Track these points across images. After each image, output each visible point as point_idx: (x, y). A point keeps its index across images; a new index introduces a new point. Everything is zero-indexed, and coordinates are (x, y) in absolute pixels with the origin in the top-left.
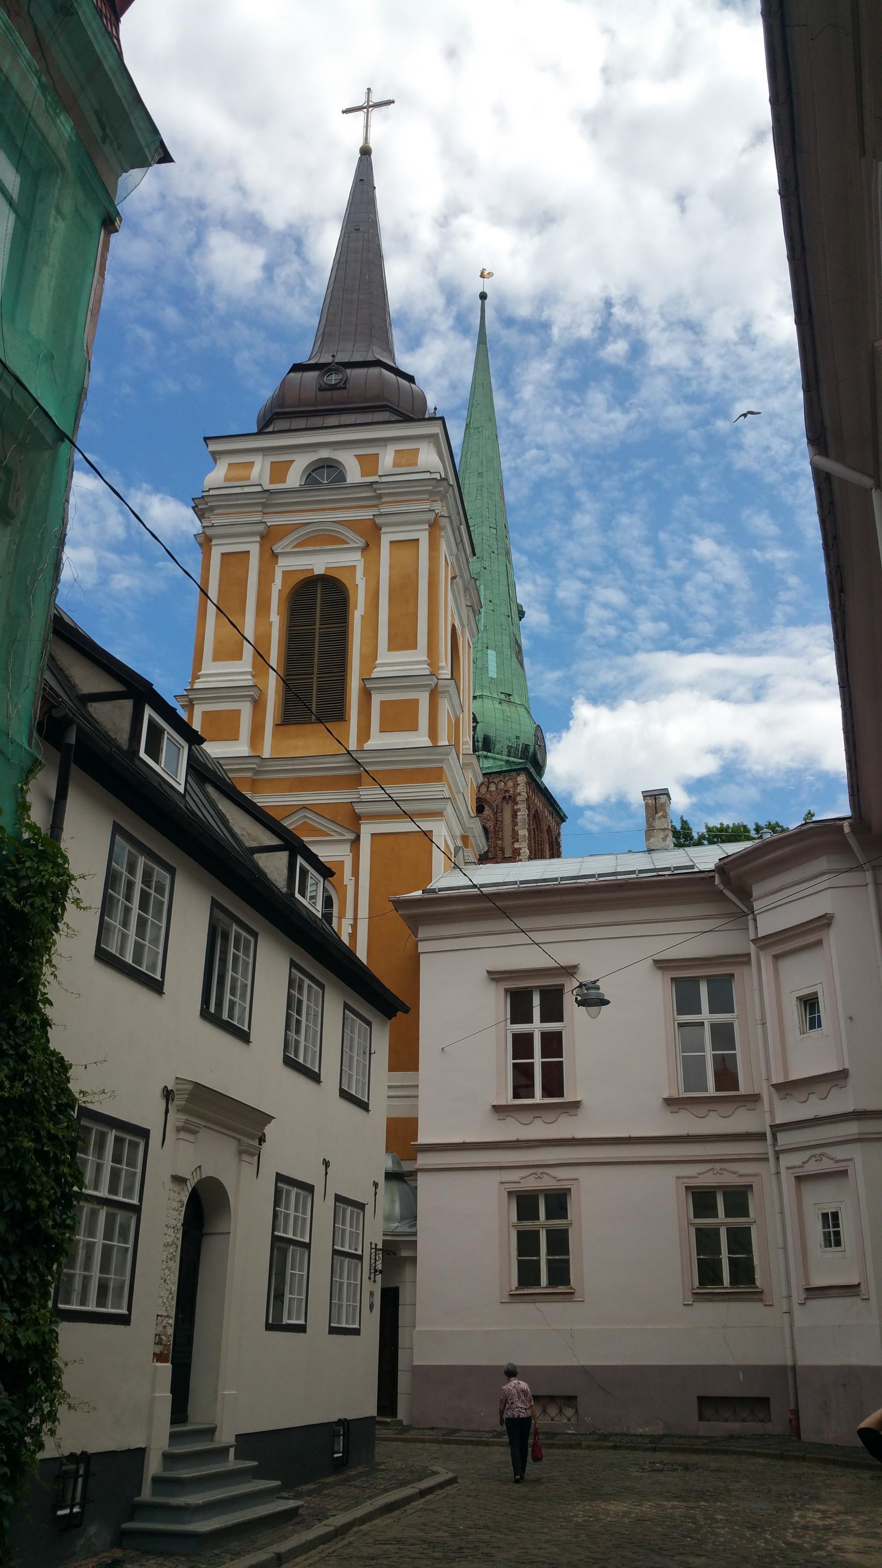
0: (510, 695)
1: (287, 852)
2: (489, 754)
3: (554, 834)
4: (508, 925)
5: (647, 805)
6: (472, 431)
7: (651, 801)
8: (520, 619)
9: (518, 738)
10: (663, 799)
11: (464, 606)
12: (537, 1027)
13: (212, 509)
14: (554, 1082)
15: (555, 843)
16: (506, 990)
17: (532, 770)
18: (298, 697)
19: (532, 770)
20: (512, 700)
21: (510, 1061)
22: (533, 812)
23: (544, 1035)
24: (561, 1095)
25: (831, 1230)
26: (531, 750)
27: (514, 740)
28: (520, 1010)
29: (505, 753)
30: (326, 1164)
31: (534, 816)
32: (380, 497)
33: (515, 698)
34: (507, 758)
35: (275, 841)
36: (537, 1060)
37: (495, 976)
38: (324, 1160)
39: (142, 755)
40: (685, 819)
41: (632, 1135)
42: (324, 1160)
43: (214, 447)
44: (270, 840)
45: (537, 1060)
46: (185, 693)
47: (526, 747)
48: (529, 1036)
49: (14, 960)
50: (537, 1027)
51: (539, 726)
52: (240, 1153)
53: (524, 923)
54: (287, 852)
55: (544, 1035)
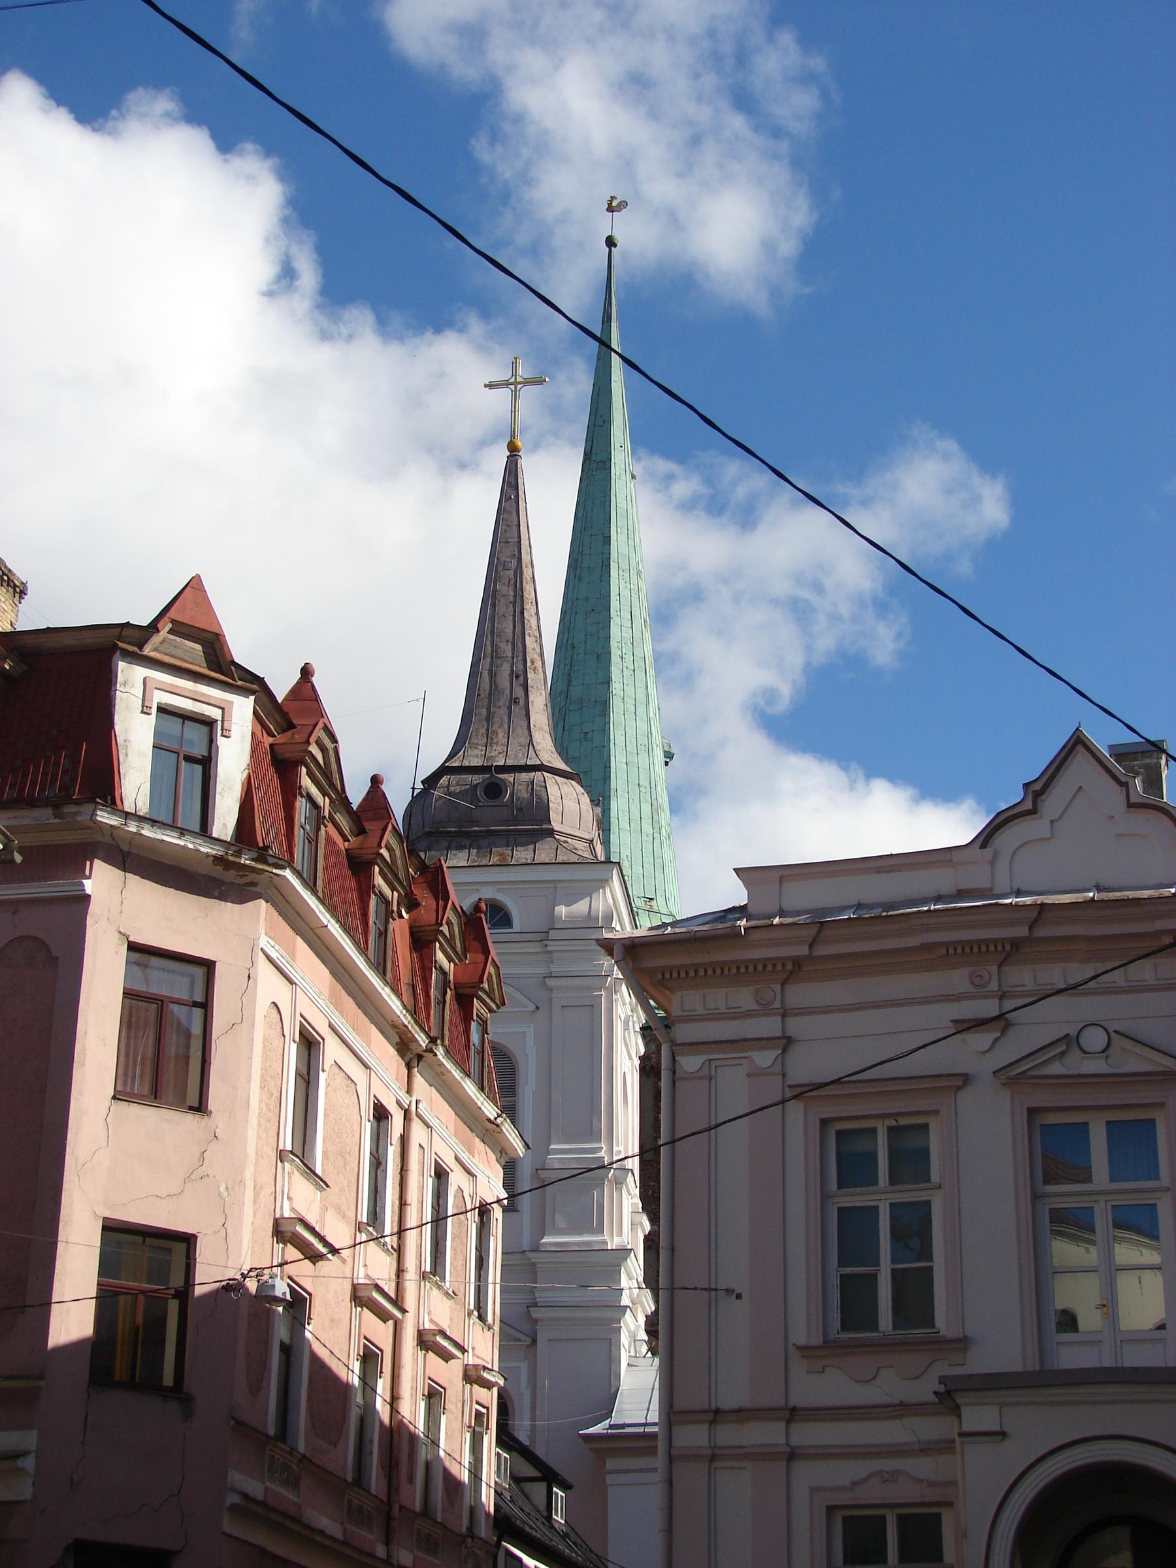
0: (651, 899)
25: (881, 1198)
50: (881, 1198)
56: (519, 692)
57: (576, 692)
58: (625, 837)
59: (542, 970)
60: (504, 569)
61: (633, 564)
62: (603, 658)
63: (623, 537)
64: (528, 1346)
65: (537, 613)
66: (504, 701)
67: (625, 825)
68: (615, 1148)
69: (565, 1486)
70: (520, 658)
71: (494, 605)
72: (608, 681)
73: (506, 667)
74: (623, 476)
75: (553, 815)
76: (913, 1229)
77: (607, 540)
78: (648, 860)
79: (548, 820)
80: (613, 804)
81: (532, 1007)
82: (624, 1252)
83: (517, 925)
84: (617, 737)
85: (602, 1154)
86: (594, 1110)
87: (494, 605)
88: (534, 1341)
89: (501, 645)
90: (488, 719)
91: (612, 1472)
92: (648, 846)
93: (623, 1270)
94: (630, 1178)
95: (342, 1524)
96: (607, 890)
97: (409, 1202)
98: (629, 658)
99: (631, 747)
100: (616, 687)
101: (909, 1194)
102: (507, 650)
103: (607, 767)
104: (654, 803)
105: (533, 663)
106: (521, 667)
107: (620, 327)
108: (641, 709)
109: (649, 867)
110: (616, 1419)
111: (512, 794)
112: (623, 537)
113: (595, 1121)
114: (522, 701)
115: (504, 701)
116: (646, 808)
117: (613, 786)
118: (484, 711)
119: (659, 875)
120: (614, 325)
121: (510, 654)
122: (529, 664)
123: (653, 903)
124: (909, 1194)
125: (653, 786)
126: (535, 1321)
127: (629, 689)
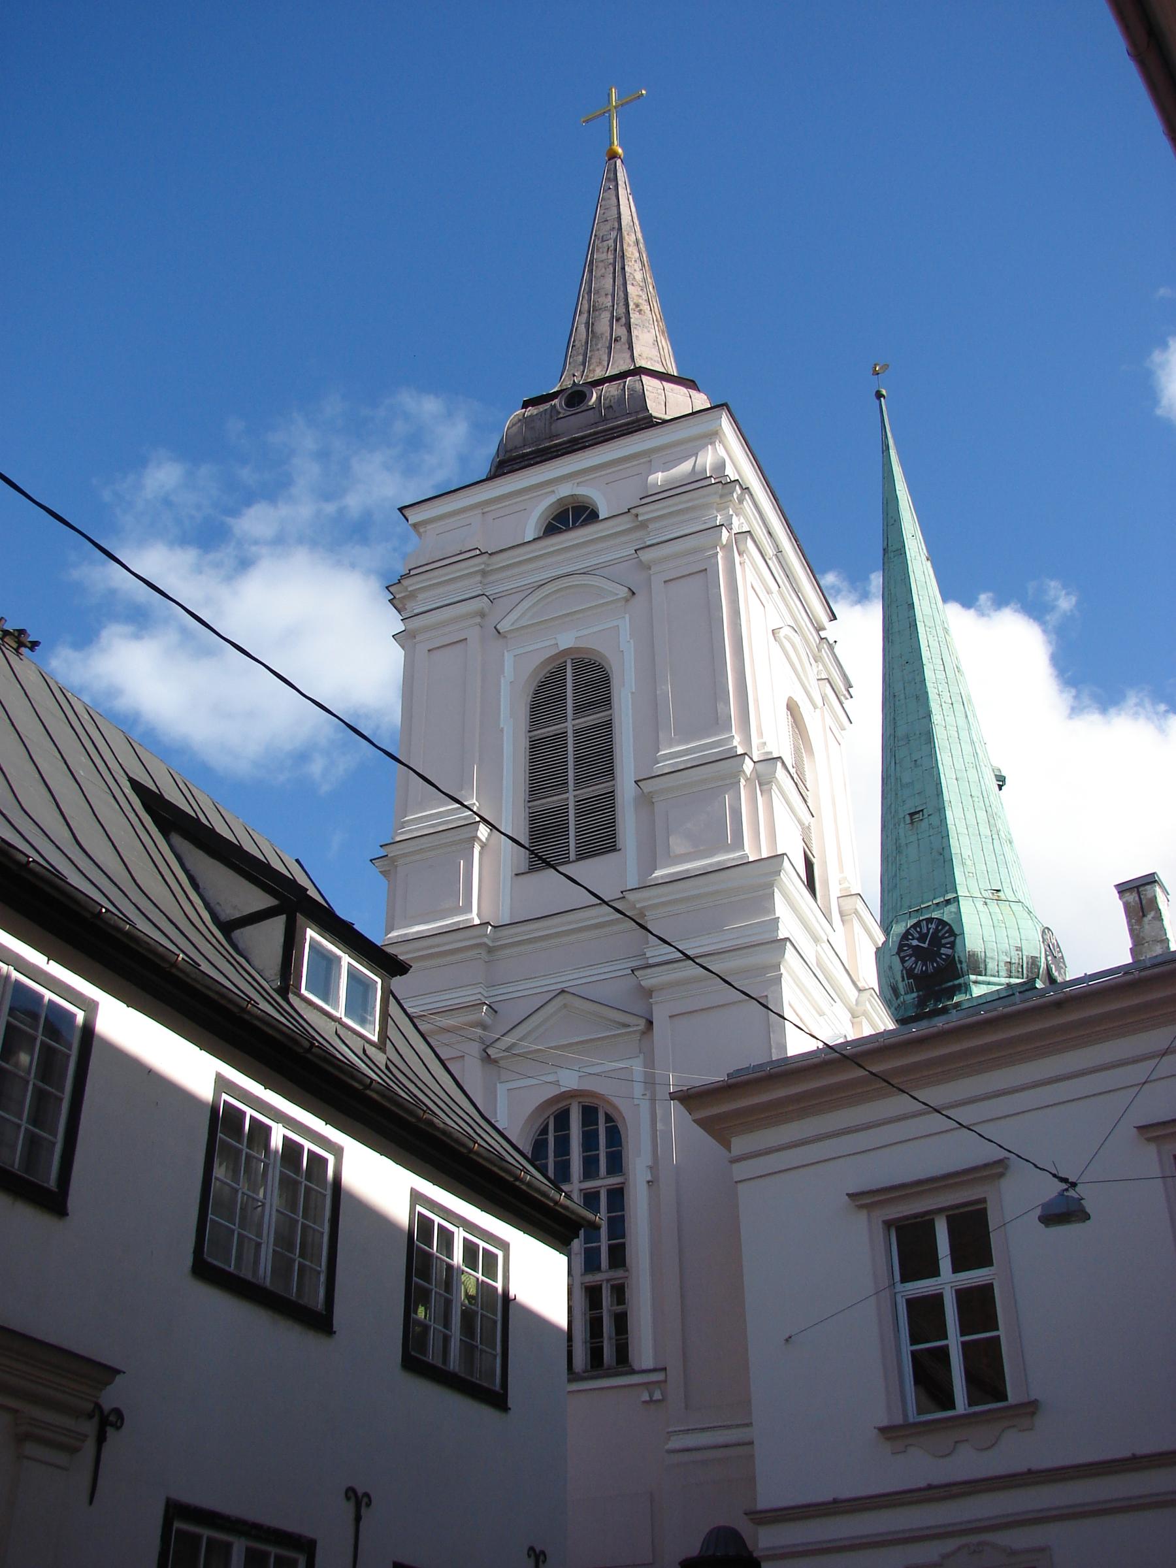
0: (998, 891)
2: (980, 978)
4: (899, 1104)
5: (1127, 907)
6: (892, 555)
7: (1132, 897)
8: (1000, 787)
9: (1019, 949)
10: (1148, 891)
11: (814, 682)
12: (947, 1281)
13: (412, 595)
14: (987, 1379)
16: (888, 1224)
20: (1003, 897)
23: (933, 1271)
26: (1043, 965)
27: (1014, 953)
28: (915, 1256)
29: (1003, 973)
30: (358, 1500)
32: (643, 525)
33: (1007, 893)
34: (1007, 980)
36: (954, 1341)
37: (864, 1200)
38: (532, 1549)
39: (379, 981)
42: (532, 1549)
43: (415, 516)
45: (954, 1341)
46: (382, 852)
47: (1034, 961)
48: (938, 1299)
50: (947, 1281)
52: (21, 1438)
53: (935, 1095)
55: (965, 1297)
56: (620, 331)
57: (901, 732)
58: (964, 840)
60: (603, 241)
61: (938, 622)
62: (922, 697)
63: (925, 603)
64: (643, 1033)
66: (603, 344)
67: (962, 829)
70: (622, 304)
71: (591, 271)
72: (928, 715)
73: (605, 317)
76: (978, 1307)
77: (911, 606)
78: (991, 859)
80: (949, 813)
81: (623, 592)
84: (944, 759)
86: (718, 692)
87: (591, 271)
88: (650, 1023)
90: (584, 364)
92: (988, 846)
93: (778, 896)
94: (780, 772)
98: (946, 695)
99: (959, 765)
100: (936, 718)
101: (974, 1277)
103: (939, 784)
104: (989, 809)
106: (622, 310)
107: (899, 453)
108: (964, 735)
109: (992, 865)
112: (925, 603)
113: (720, 706)
114: (624, 339)
115: (603, 344)
116: (982, 815)
117: (946, 797)
118: (580, 358)
119: (1003, 870)
120: (893, 453)
122: (632, 306)
124: (974, 1277)
126: (648, 993)
127: (950, 719)
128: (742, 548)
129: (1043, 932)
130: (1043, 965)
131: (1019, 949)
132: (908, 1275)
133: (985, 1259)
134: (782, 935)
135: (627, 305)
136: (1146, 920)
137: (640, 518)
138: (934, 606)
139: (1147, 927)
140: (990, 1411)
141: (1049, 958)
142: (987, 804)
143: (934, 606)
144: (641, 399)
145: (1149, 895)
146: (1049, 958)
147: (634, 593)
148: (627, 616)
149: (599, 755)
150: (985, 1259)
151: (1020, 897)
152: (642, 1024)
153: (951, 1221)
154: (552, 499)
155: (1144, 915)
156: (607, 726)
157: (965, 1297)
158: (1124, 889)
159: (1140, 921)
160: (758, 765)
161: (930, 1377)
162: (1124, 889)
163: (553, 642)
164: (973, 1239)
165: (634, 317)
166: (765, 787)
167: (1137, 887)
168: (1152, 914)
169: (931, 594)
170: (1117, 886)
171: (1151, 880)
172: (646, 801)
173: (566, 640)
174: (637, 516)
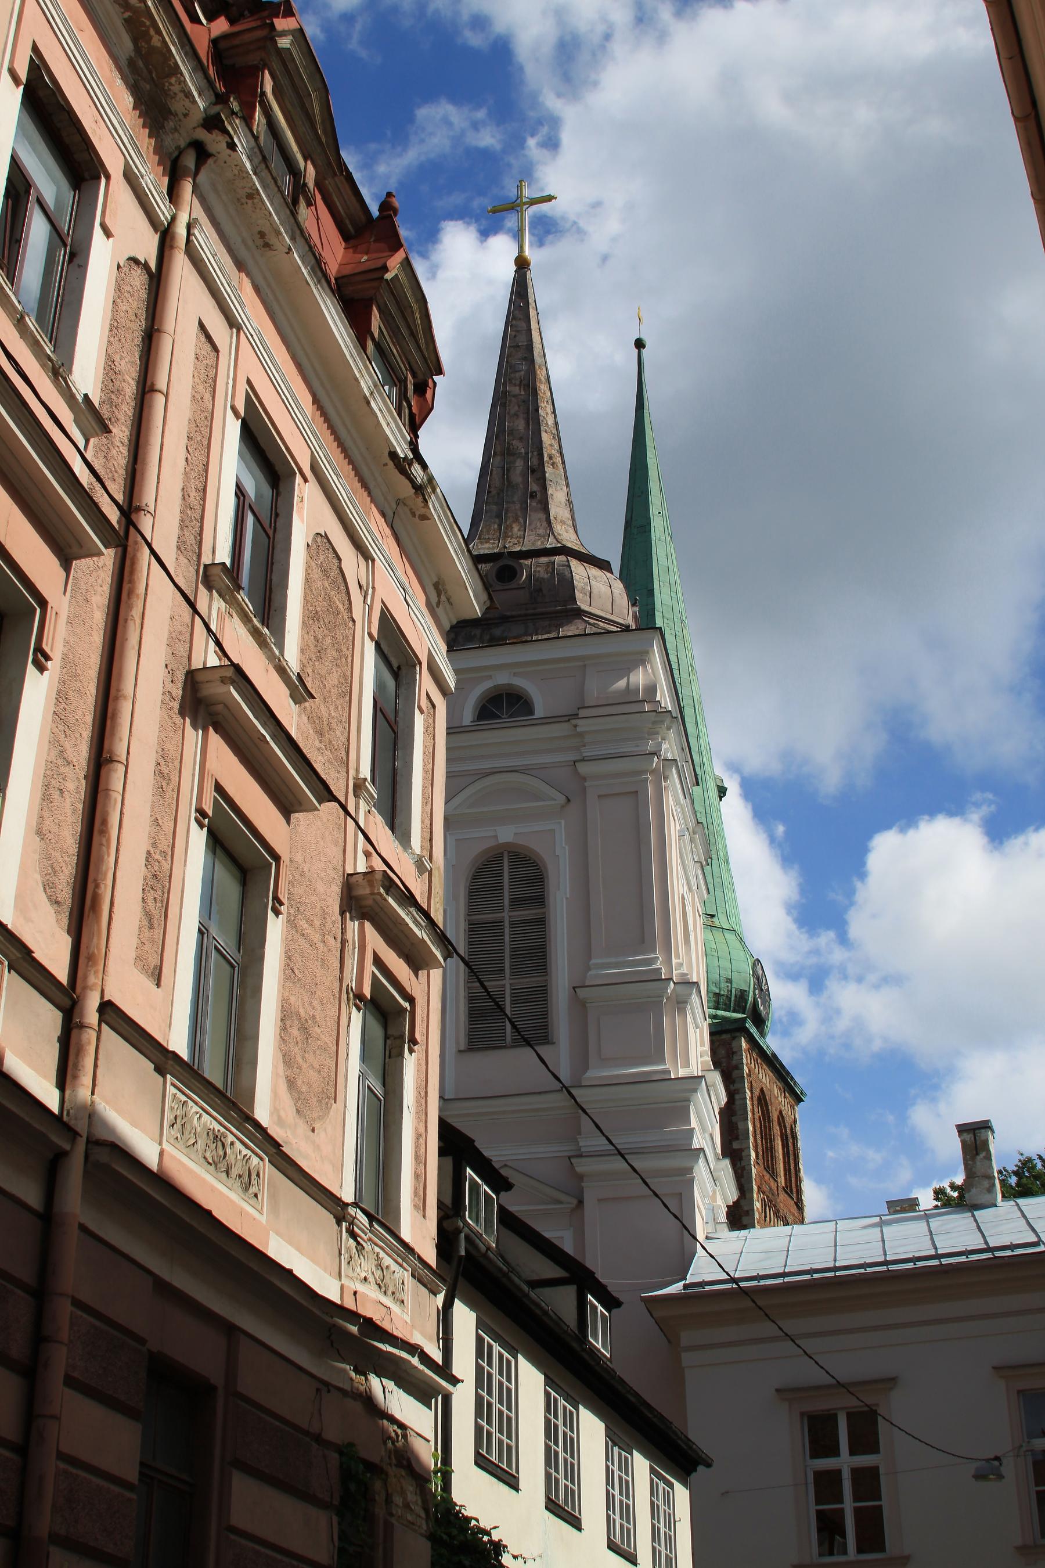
0: (712, 916)
1: (575, 1287)
3: (788, 1121)
5: (963, 1143)
7: (968, 1137)
8: (721, 799)
9: (729, 981)
15: (789, 1136)
16: (802, 1414)
17: (753, 1030)
18: (523, 1037)
19: (753, 1030)
20: (717, 924)
21: (813, 1508)
22: (757, 1093)
24: (882, 1549)
25: (845, 1462)
26: (750, 999)
27: (724, 985)
28: (821, 1442)
31: (759, 1099)
33: (721, 921)
35: (558, 1273)
36: (848, 1505)
40: (396, 202)
41: (215, 1213)
44: (551, 1270)
45: (848, 1505)
49: (486, 1538)
50: (845, 1462)
51: (758, 960)
54: (575, 1287)
55: (857, 1473)
56: (533, 487)
59: (571, 756)
63: (665, 590)
65: (554, 412)
68: (674, 961)
69: (611, 1302)
74: (663, 538)
75: (578, 595)
76: (867, 1482)
79: (574, 599)
81: (562, 799)
82: (695, 1080)
83: (539, 712)
85: (658, 965)
88: (581, 1202)
89: (514, 442)
91: (690, 1348)
94: (694, 997)
95: (160, 1144)
96: (648, 667)
97: (161, 383)
101: (865, 1460)
102: (520, 447)
105: (551, 458)
110: (690, 1279)
111: (529, 576)
112: (665, 590)
121: (523, 450)
122: (546, 458)
123: (715, 919)
124: (865, 1460)
125: (708, 811)
126: (580, 1177)
128: (667, 773)
129: (754, 964)
130: (750, 999)
131: (729, 981)
132: (815, 1454)
133: (873, 1447)
134: (696, 1145)
135: (541, 455)
136: (978, 1158)
137: (578, 729)
138: (674, 595)
139: (978, 1163)
140: (877, 1560)
141: (757, 992)
142: (709, 821)
143: (674, 595)
144: (569, 584)
145: (983, 1138)
146: (757, 992)
147: (569, 800)
148: (563, 822)
149: (535, 955)
150: (873, 1447)
151: (735, 928)
152: (575, 1202)
153: (849, 1416)
154: (488, 685)
155: (977, 1154)
156: (541, 922)
157: (857, 1473)
158: (962, 1129)
159: (973, 1159)
160: (677, 986)
161: (829, 1528)
162: (962, 1129)
163: (492, 834)
164: (866, 1434)
165: (549, 470)
166: (681, 1005)
167: (974, 1130)
168: (983, 1155)
169: (672, 582)
170: (958, 1126)
171: (986, 1126)
172: (580, 1006)
173: (506, 834)
174: (575, 726)
